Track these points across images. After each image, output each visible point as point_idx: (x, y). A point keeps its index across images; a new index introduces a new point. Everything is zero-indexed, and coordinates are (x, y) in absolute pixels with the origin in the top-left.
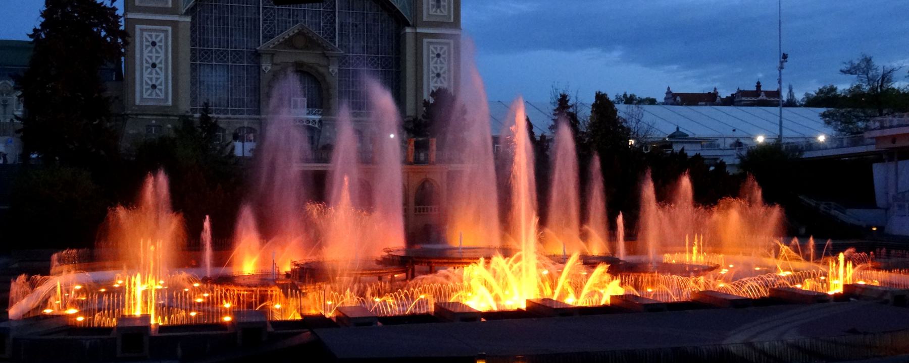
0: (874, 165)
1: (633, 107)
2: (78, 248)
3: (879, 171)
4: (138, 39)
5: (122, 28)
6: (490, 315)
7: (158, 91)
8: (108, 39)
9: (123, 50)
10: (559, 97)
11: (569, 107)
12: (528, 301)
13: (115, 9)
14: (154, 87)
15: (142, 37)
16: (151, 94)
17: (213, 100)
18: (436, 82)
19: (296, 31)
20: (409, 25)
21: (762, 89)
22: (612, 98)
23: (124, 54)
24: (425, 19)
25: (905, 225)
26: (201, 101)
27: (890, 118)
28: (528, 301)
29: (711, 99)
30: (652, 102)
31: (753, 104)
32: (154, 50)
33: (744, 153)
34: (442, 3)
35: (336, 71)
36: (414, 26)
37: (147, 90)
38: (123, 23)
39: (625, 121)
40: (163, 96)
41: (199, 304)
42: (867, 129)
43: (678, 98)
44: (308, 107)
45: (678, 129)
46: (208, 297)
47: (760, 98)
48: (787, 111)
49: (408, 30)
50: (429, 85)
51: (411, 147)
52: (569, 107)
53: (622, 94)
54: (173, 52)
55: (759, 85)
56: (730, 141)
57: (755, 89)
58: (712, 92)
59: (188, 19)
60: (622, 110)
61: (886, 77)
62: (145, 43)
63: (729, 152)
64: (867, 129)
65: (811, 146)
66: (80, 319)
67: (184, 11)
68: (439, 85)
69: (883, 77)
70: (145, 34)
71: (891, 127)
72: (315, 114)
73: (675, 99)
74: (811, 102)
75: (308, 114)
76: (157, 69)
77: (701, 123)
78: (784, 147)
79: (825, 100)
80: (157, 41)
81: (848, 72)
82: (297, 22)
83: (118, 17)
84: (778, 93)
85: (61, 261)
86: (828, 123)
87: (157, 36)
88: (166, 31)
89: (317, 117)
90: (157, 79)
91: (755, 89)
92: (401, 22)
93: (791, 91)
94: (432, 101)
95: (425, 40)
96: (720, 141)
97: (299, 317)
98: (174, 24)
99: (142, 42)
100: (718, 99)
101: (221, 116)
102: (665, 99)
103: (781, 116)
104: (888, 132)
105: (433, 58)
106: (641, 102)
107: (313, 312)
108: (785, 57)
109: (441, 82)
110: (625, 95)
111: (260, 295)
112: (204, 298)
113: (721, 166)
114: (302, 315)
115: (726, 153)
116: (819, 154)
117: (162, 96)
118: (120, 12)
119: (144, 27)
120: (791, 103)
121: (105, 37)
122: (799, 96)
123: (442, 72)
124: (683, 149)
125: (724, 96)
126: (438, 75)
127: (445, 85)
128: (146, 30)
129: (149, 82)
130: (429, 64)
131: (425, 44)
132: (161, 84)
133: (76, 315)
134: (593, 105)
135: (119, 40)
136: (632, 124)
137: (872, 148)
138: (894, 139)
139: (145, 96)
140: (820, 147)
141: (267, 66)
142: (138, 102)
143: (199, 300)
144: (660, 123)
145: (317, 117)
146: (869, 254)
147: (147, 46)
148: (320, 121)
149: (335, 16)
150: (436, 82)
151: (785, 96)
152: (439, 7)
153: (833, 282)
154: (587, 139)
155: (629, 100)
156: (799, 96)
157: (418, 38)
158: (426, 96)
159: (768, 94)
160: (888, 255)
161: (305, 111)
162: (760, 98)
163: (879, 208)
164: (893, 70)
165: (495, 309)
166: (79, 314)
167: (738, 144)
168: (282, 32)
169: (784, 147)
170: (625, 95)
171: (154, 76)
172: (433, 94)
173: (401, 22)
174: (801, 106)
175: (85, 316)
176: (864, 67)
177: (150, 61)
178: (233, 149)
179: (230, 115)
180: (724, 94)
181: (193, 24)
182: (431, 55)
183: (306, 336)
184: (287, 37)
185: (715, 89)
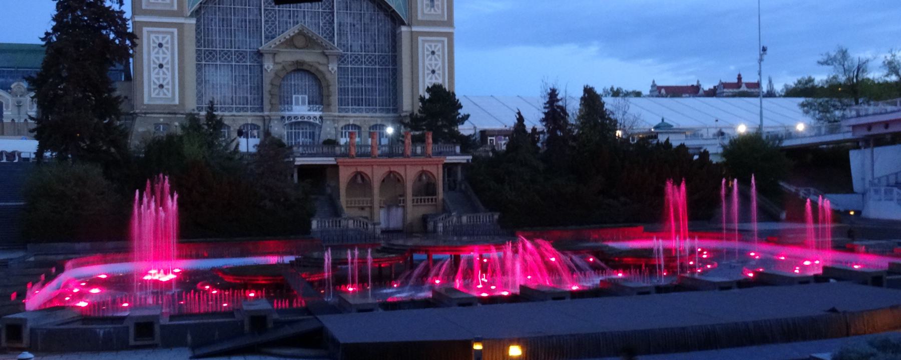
1: (619, 99)
3: (856, 158)
5: (130, 30)
8: (117, 41)
10: (549, 91)
11: (558, 100)
13: (122, 12)
15: (149, 39)
17: (218, 98)
18: (431, 78)
19: (297, 31)
20: (403, 24)
23: (132, 56)
25: (883, 209)
29: (694, 91)
30: (638, 94)
31: (734, 95)
35: (336, 69)
39: (612, 113)
40: (170, 96)
42: (844, 117)
43: (663, 91)
48: (767, 102)
49: (404, 29)
52: (558, 100)
55: (739, 78)
57: (736, 81)
58: (695, 84)
59: (193, 21)
60: (609, 103)
63: (713, 142)
67: (189, 14)
68: (434, 81)
71: (866, 115)
74: (791, 93)
75: (309, 110)
79: (803, 90)
83: (125, 20)
84: (758, 85)
89: (318, 114)
91: (736, 81)
92: (396, 20)
94: (427, 96)
95: (420, 39)
96: (704, 132)
98: (180, 27)
100: (701, 92)
101: (226, 113)
104: (863, 121)
106: (627, 94)
108: (764, 49)
110: (612, 89)
113: (705, 155)
115: (709, 142)
117: (169, 95)
118: (128, 15)
120: (771, 94)
121: (114, 39)
122: (779, 87)
124: (668, 139)
127: (439, 81)
134: (582, 99)
135: (128, 42)
136: (619, 116)
137: (849, 136)
138: (869, 126)
141: (269, 65)
148: (321, 117)
149: (333, 16)
156: (779, 87)
157: (413, 36)
167: (721, 134)
170: (612, 89)
173: (396, 20)
174: (780, 96)
179: (234, 113)
180: (707, 86)
181: (198, 26)
185: (698, 82)
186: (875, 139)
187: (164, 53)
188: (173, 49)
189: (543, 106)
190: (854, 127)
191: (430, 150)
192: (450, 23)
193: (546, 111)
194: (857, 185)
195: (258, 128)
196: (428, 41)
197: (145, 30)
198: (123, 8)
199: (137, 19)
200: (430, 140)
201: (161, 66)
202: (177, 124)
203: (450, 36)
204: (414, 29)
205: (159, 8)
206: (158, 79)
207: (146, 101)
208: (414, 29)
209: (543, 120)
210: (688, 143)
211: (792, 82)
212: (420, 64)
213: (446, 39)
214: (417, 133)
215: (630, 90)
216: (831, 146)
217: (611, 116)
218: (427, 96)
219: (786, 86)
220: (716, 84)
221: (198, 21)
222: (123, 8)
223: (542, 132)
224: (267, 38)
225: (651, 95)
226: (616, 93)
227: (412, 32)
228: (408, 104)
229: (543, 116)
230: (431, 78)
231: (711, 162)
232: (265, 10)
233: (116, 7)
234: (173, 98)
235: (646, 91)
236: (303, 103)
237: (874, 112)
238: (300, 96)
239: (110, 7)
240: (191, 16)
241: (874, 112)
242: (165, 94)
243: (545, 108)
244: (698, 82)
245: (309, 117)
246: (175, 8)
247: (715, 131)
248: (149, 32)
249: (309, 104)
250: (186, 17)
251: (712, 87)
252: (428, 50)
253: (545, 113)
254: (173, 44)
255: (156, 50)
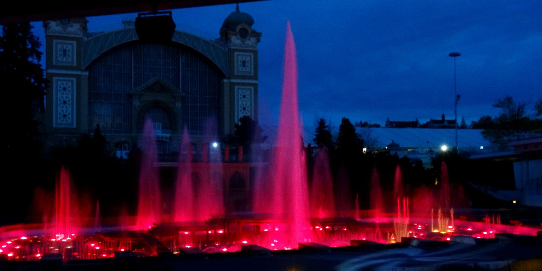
0: (515, 164)
1: (366, 129)
3: (517, 167)
4: (54, 86)
5: (45, 77)
7: (67, 119)
8: (36, 84)
10: (319, 121)
11: (325, 127)
12: (300, 244)
13: (40, 65)
14: (65, 116)
15: (57, 84)
16: (67, 47)
17: (102, 124)
18: (243, 113)
19: (155, 81)
20: (225, 78)
21: (446, 118)
23: (46, 94)
24: (236, 74)
25: (535, 201)
27: (523, 134)
29: (414, 124)
30: (378, 126)
31: (439, 127)
33: (434, 156)
35: (180, 106)
36: (229, 78)
39: (361, 136)
40: (71, 121)
42: (510, 141)
43: (394, 125)
45: (393, 141)
48: (460, 132)
49: (225, 80)
51: (227, 152)
52: (325, 127)
54: (77, 105)
55: (443, 117)
57: (441, 119)
58: (415, 120)
59: (87, 73)
60: (358, 130)
61: (521, 109)
63: (425, 156)
64: (510, 141)
65: (476, 151)
67: (84, 69)
68: (244, 114)
69: (519, 109)
70: (59, 83)
71: (524, 139)
72: (167, 133)
73: (391, 124)
74: (475, 126)
75: (163, 133)
76: (67, 105)
77: (410, 142)
79: (485, 125)
80: (67, 86)
83: (42, 70)
84: (454, 122)
89: (168, 135)
90: (67, 111)
91: (441, 119)
92: (221, 75)
93: (463, 120)
94: (240, 124)
95: (236, 87)
96: (419, 150)
98: (78, 77)
99: (57, 87)
100: (418, 125)
101: (108, 134)
104: (522, 143)
105: (241, 98)
106: (371, 126)
108: (458, 97)
110: (361, 123)
113: (419, 163)
115: (422, 156)
117: (70, 122)
118: (44, 67)
120: (463, 127)
121: (34, 83)
122: (468, 123)
123: (246, 107)
124: (396, 153)
126: (244, 109)
127: (248, 114)
129: (62, 113)
130: (238, 103)
131: (236, 90)
132: (69, 101)
134: (341, 126)
135: (43, 85)
136: (365, 138)
137: (512, 153)
138: (526, 146)
139: (59, 121)
141: (136, 103)
144: (383, 138)
145: (168, 135)
148: (170, 138)
149: (179, 72)
154: (337, 147)
156: (468, 123)
157: (232, 85)
158: (236, 121)
163: (456, 118)
164: (524, 105)
167: (431, 151)
170: (361, 123)
171: (65, 96)
172: (241, 120)
173: (221, 75)
174: (469, 128)
177: (62, 86)
178: (115, 154)
179: (113, 134)
180: (422, 122)
181: (90, 76)
182: (240, 96)
185: (417, 119)
186: (528, 154)
187: (67, 94)
188: (73, 91)
189: (315, 131)
190: (515, 146)
191: (241, 158)
192: (255, 77)
193: (318, 134)
194: (518, 184)
195: (129, 143)
196: (241, 89)
197: (55, 78)
198: (41, 63)
199: (50, 71)
200: (242, 152)
201: (65, 102)
202: (74, 140)
203: (255, 86)
204: (233, 81)
205: (64, 64)
206: (62, 111)
207: (54, 125)
208: (233, 81)
209: (315, 140)
210: (409, 156)
211: (476, 120)
212: (236, 104)
213: (253, 88)
214: (233, 148)
215: (372, 123)
216: (501, 160)
217: (359, 138)
218: (240, 124)
219: (473, 122)
220: (428, 120)
221: (90, 73)
222: (41, 63)
223: (315, 148)
224: (135, 85)
225: (387, 126)
226: (364, 125)
227: (231, 83)
228: (227, 130)
229: (315, 137)
230: (243, 113)
231: (424, 168)
232: (135, 67)
233: (35, 61)
234: (73, 61)
235: (383, 124)
236: (159, 128)
237: (527, 138)
238: (157, 124)
239: (32, 62)
240: (86, 70)
241: (527, 138)
242: (67, 121)
243: (317, 132)
244: (417, 119)
245: (162, 137)
246: (75, 64)
247: (427, 150)
248: (57, 80)
249: (162, 128)
250: (82, 71)
251: (425, 122)
252: (241, 95)
253: (316, 135)
254: (73, 115)
255: (62, 92)
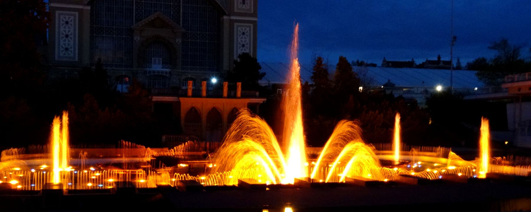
1: (363, 68)
2: (18, 148)
5: (47, 10)
6: (272, 186)
8: (39, 17)
9: (48, 24)
15: (60, 18)
20: (225, 14)
21: (442, 59)
22: (350, 61)
24: (236, 11)
26: (96, 59)
28: (295, 179)
30: (374, 65)
32: (67, 27)
34: (246, 1)
35: (181, 41)
36: (229, 15)
37: (62, 51)
38: (48, 8)
41: (93, 179)
44: (163, 63)
45: (389, 81)
46: (99, 176)
47: (440, 65)
49: (225, 17)
50: (237, 51)
53: (355, 61)
56: (421, 90)
60: (355, 69)
62: (62, 22)
63: (420, 95)
64: (504, 82)
66: (19, 187)
67: (86, 3)
68: (243, 51)
71: (518, 81)
72: (167, 68)
73: (387, 64)
74: (470, 67)
75: (163, 68)
76: (69, 38)
78: (453, 92)
81: (494, 48)
82: (157, 11)
85: (7, 154)
86: (480, 79)
87: (69, 18)
88: (75, 16)
89: (168, 70)
95: (236, 24)
97: (156, 187)
98: (80, 11)
99: (59, 21)
101: (109, 68)
102: (382, 65)
103: (451, 75)
106: (367, 65)
107: (164, 183)
108: (455, 38)
109: (245, 50)
110: (358, 62)
111: (131, 174)
112: (96, 176)
114: (157, 185)
116: (473, 97)
117: (72, 55)
119: (61, 12)
120: (459, 68)
124: (392, 92)
125: (418, 64)
128: (62, 14)
131: (235, 26)
133: (17, 185)
134: (338, 64)
135: (46, 18)
140: (475, 93)
142: (56, 59)
143: (94, 177)
145: (168, 70)
146: (502, 158)
147: (63, 24)
148: (170, 73)
149: (180, 8)
150: (242, 50)
151: (454, 63)
152: (244, 3)
153: (480, 172)
155: (360, 64)
156: (464, 63)
158: (235, 57)
159: (445, 62)
160: (514, 159)
161: (161, 66)
162: (440, 65)
165: (275, 183)
166: (19, 184)
167: (426, 92)
168: (147, 17)
169: (453, 92)
170: (358, 62)
172: (240, 56)
174: (464, 69)
175: (22, 185)
176: (502, 45)
178: (116, 87)
179: (114, 68)
180: (419, 61)
183: (159, 196)
184: (150, 20)
